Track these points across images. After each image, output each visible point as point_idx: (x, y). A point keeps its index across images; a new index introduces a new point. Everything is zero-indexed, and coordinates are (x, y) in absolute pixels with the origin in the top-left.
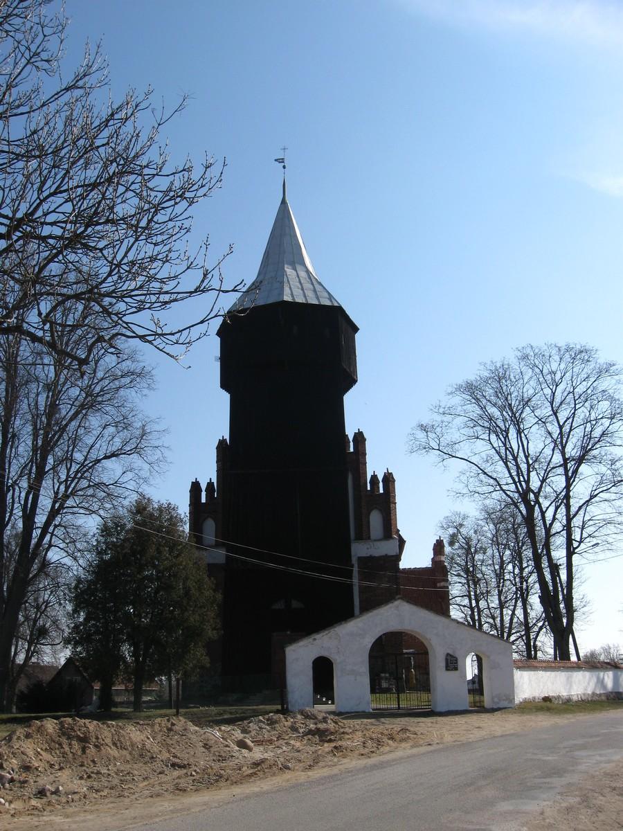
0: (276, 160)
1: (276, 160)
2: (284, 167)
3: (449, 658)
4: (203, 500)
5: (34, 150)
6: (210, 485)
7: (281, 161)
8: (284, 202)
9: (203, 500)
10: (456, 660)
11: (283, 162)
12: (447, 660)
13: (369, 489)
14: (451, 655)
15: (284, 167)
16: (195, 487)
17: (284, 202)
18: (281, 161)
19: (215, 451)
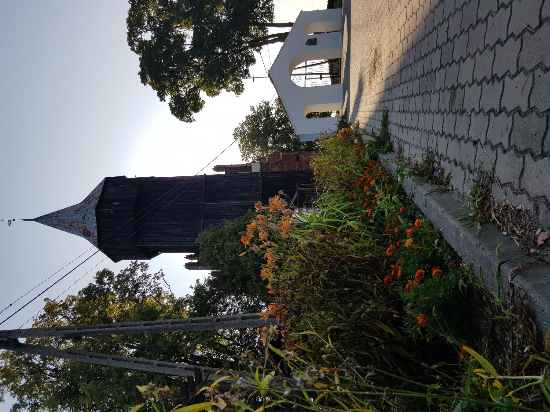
0: (9, 226)
1: (9, 226)
2: (14, 220)
3: (308, 43)
4: (196, 261)
5: (171, 401)
6: (188, 257)
7: (10, 222)
8: (36, 220)
9: (196, 261)
10: (310, 39)
11: (11, 221)
12: (309, 45)
13: (224, 173)
14: (307, 42)
15: (14, 220)
16: (189, 266)
17: (36, 220)
18: (10, 222)
19: (192, 271)
